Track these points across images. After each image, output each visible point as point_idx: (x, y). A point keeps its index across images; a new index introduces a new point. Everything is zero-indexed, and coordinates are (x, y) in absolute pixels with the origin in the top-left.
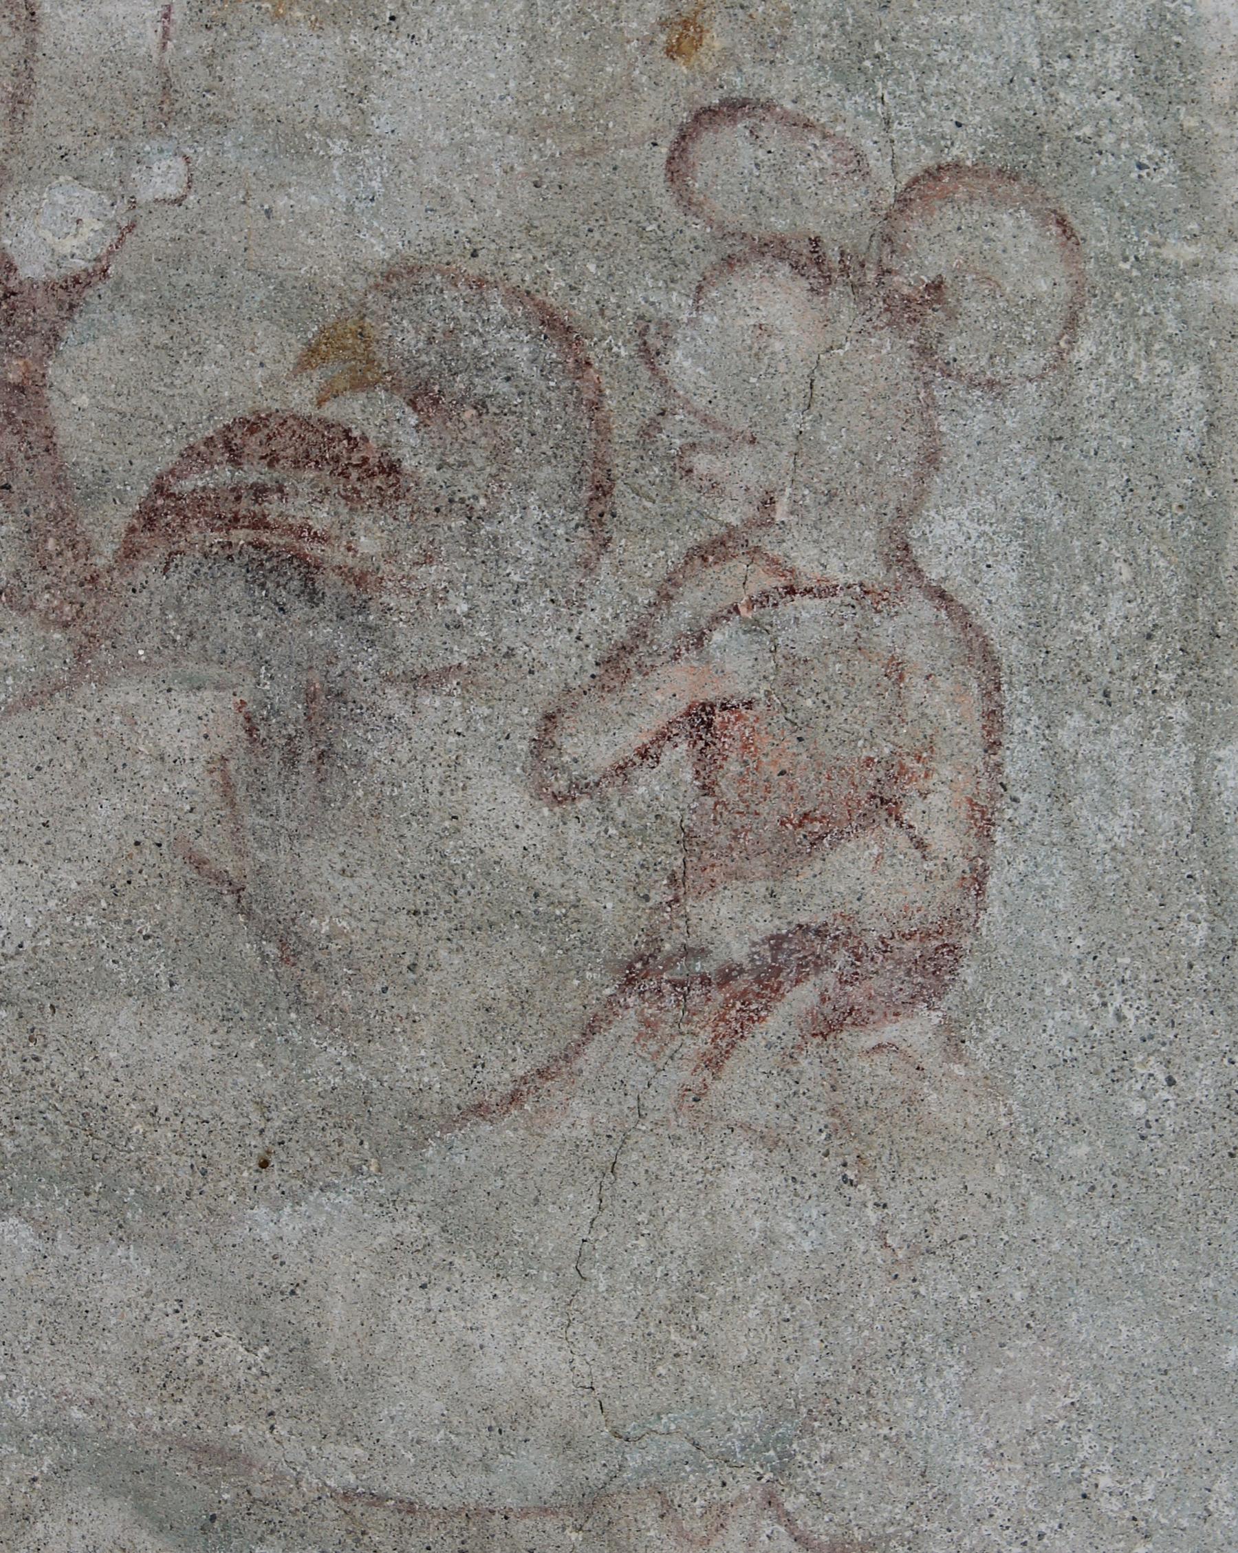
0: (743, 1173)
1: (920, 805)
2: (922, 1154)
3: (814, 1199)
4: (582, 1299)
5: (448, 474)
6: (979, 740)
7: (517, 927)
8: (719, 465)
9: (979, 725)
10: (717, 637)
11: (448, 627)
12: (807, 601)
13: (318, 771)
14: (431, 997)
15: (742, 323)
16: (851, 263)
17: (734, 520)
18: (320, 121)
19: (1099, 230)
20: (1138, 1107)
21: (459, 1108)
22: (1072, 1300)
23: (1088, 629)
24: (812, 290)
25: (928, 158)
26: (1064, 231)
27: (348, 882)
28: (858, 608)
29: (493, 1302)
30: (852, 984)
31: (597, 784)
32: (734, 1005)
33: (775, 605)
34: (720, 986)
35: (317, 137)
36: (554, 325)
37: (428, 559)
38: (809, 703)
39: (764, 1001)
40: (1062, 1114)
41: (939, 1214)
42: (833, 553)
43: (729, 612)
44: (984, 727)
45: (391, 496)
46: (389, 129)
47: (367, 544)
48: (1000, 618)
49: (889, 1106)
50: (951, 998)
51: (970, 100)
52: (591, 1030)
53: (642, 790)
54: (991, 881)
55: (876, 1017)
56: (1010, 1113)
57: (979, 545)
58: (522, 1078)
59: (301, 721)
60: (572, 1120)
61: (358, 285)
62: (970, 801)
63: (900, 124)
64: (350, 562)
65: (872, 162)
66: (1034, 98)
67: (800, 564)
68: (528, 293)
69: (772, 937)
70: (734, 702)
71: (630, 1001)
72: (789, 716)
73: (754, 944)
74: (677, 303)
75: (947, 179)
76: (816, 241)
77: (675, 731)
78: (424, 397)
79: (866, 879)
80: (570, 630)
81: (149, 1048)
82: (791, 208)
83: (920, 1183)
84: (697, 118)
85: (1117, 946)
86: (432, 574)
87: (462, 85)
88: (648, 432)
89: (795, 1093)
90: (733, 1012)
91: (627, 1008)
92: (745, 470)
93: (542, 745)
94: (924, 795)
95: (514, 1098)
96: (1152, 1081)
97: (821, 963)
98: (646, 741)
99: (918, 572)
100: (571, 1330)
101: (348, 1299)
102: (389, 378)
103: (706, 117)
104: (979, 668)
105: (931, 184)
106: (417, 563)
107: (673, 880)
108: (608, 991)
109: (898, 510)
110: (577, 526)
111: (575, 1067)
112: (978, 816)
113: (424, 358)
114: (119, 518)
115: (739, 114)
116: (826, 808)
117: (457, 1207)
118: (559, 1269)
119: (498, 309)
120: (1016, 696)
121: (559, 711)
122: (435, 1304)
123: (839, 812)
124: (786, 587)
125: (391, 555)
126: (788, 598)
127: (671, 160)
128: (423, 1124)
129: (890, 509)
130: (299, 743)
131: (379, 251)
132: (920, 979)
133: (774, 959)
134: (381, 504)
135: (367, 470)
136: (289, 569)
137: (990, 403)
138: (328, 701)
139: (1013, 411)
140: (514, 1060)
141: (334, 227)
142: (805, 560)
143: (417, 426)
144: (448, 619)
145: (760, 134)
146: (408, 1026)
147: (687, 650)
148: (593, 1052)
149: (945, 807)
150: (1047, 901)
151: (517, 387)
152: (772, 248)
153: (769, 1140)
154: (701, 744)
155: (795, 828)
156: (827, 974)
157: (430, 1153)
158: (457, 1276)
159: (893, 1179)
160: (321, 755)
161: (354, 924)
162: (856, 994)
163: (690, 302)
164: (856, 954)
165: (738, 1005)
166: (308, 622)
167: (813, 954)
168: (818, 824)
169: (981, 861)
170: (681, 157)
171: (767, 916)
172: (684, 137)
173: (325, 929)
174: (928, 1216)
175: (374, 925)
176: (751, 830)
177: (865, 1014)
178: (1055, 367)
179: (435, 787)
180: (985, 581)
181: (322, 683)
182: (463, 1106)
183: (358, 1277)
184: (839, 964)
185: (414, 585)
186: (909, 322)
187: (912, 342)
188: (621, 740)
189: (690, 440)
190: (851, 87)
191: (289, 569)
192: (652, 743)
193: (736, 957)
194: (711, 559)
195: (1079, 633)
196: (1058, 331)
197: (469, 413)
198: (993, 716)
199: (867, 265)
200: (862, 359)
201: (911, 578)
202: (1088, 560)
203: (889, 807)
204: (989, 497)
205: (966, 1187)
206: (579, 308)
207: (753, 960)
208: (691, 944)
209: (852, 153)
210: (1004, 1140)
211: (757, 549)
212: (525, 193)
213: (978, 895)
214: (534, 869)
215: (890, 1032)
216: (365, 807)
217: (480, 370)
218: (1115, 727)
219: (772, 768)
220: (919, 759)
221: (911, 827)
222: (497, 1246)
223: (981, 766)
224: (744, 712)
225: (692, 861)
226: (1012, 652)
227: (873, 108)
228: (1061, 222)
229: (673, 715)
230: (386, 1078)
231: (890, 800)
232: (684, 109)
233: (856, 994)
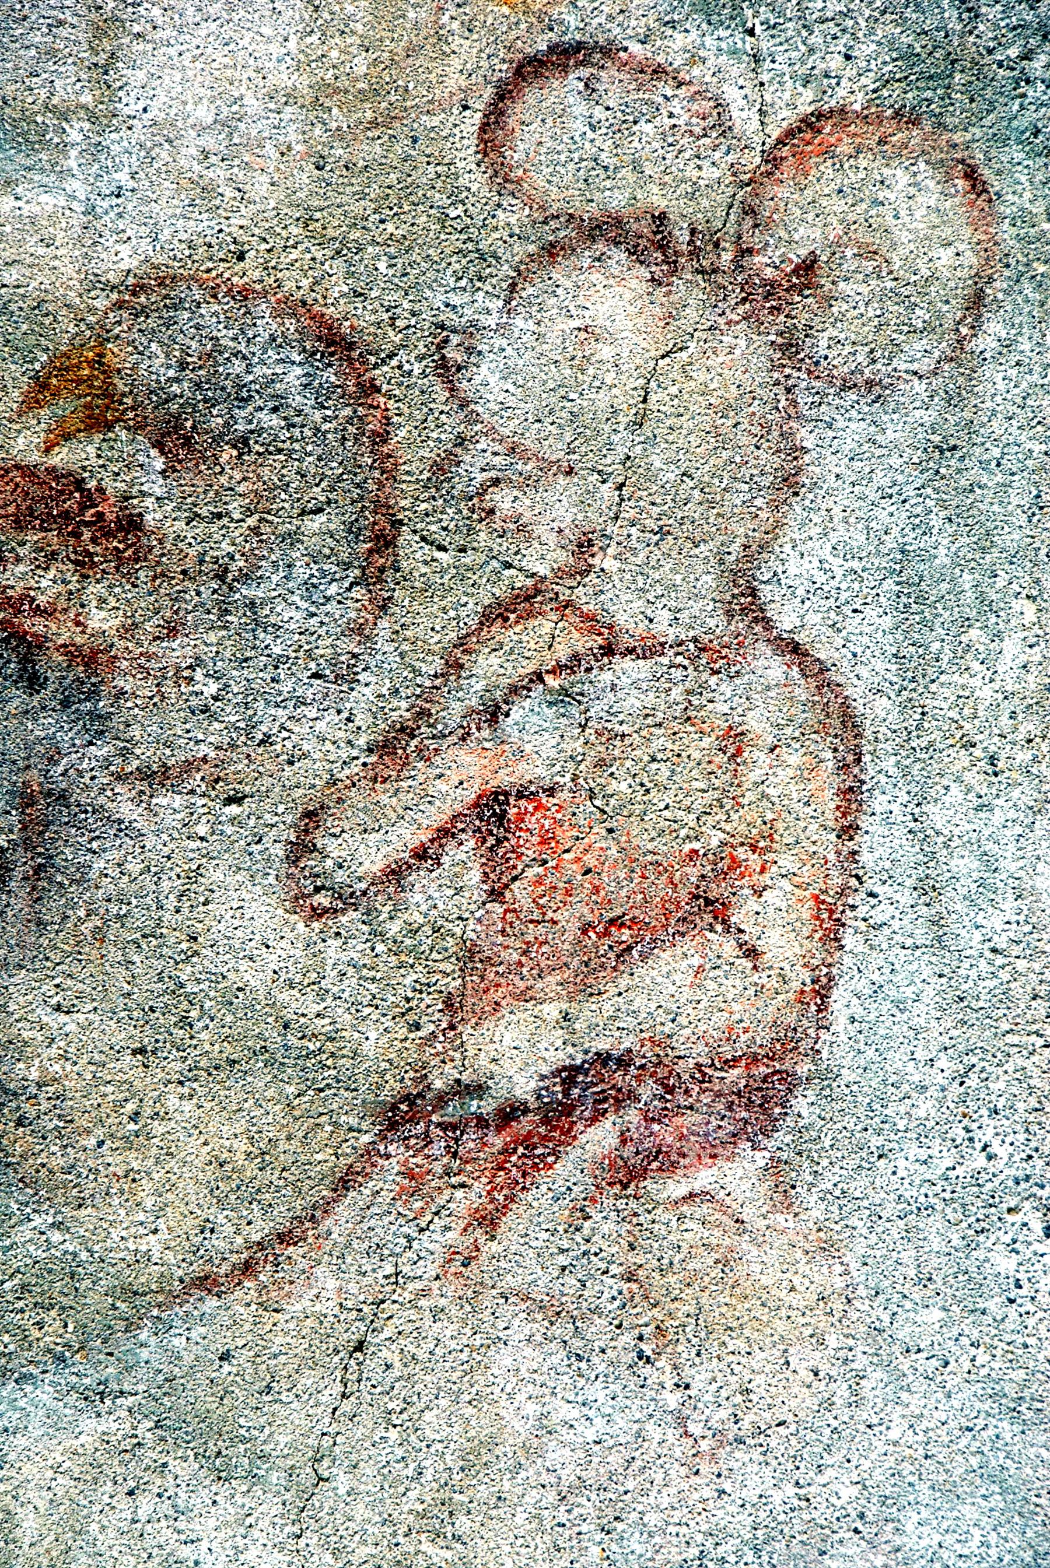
0: (521, 1352)
1: (753, 905)
2: (735, 1324)
3: (601, 1379)
4: (317, 1505)
5: (200, 528)
6: (831, 824)
7: (261, 1064)
8: (528, 502)
9: (832, 805)
10: (516, 714)
11: (193, 713)
12: (628, 663)
13: (34, 888)
14: (154, 1150)
15: (562, 326)
16: (705, 239)
17: (542, 570)
18: (55, 101)
20: (1006, 1264)
21: (181, 1281)
22: (911, 1498)
23: (976, 682)
24: (653, 280)
25: (806, 101)
26: (974, 186)
27: (63, 1018)
28: (691, 668)
29: (213, 1510)
30: (660, 1122)
31: (364, 893)
32: (515, 1150)
33: (589, 670)
34: (499, 1129)
35: (51, 120)
36: (333, 343)
37: (172, 632)
38: (623, 787)
39: (551, 1145)
40: (912, 1273)
41: (752, 1396)
42: (656, 594)
43: (531, 681)
44: (838, 807)
45: (129, 559)
46: (140, 106)
47: (99, 620)
48: (868, 682)
49: (699, 1266)
50: (782, 1137)
51: (863, 24)
52: (344, 1183)
53: (418, 897)
54: (835, 994)
55: (687, 1161)
56: (847, 1272)
57: (844, 586)
58: (259, 1243)
59: (16, 830)
60: (315, 1291)
61: (97, 303)
62: (816, 897)
63: (773, 62)
64: (79, 640)
65: (735, 114)
66: (946, 15)
67: (621, 619)
68: (304, 303)
69: (564, 1068)
70: (533, 789)
71: (391, 1149)
72: (597, 803)
73: (543, 1078)
75: (827, 130)
76: (663, 216)
77: (460, 826)
78: (177, 438)
79: (681, 997)
80: (339, 712)
82: (631, 177)
83: (731, 1358)
84: (519, 72)
85: (989, 1069)
86: (178, 651)
87: (232, 46)
88: (442, 468)
89: (584, 1254)
90: (514, 1159)
91: (388, 1156)
92: (557, 511)
93: (301, 849)
94: (759, 893)
95: (248, 1268)
96: (1025, 1231)
97: (623, 1098)
98: (424, 839)
99: (767, 623)
100: (302, 1542)
101: (42, 1511)
102: (131, 415)
103: (530, 69)
104: (836, 736)
105: (808, 136)
106: (158, 638)
107: (448, 1004)
108: (366, 1139)
109: (746, 547)
110: (352, 585)
111: (322, 1229)
112: (825, 916)
113: (175, 388)
115: (572, 63)
116: (637, 912)
117: (174, 1398)
118: (292, 1467)
119: (266, 325)
120: (881, 766)
121: (322, 808)
122: (142, 1515)
123: (652, 915)
124: (601, 647)
125: (128, 630)
126: (606, 660)
127: (484, 128)
128: (143, 1303)
129: (735, 548)
131: (128, 261)
132: (744, 1114)
133: (566, 1093)
134: (117, 569)
135: (101, 528)
137: (866, 409)
139: (895, 417)
140: (249, 1223)
143: (164, 471)
144: (194, 702)
145: (597, 86)
146: (126, 1187)
147: (479, 729)
148: (343, 1210)
149: (784, 906)
150: (905, 1017)
151: (285, 419)
153: (553, 1311)
154: (491, 841)
155: (599, 937)
156: (633, 1112)
157: (143, 1336)
158: (171, 1480)
159: (698, 1355)
160: (38, 869)
161: (68, 1067)
162: (665, 1134)
163: (500, 303)
164: (665, 1086)
165: (521, 1150)
166: (27, 712)
167: (613, 1087)
168: (627, 931)
169: (825, 970)
170: (497, 122)
171: (559, 1043)
172: (504, 94)
173: (34, 1074)
174: (739, 1399)
175: (93, 1068)
176: (546, 942)
177: (674, 1157)
178: (952, 359)
179: (171, 903)
180: (850, 629)
181: (40, 784)
182: (187, 1279)
183: (54, 1483)
184: (644, 1098)
185: (153, 664)
186: (771, 313)
187: (772, 338)
188: (394, 838)
189: (493, 474)
190: (715, 18)
192: (432, 841)
193: (518, 1092)
194: (512, 617)
195: (964, 687)
196: (959, 314)
197: (227, 454)
198: (851, 795)
199: (723, 244)
200: (709, 362)
201: (758, 629)
202: (982, 598)
203: (718, 911)
204: (860, 526)
205: (788, 1363)
206: (364, 317)
207: (539, 1097)
208: (465, 1078)
209: (712, 104)
210: (838, 1305)
211: (568, 604)
212: (305, 177)
213: (819, 1011)
214: (284, 996)
215: (704, 1178)
216: (86, 928)
217: (243, 399)
218: (1000, 802)
219: (575, 867)
220: (754, 848)
221: (741, 931)
222: (219, 1443)
223: (832, 857)
224: (544, 801)
225: (473, 986)
226: (879, 712)
227: (740, 45)
228: (971, 174)
229: (458, 807)
230: (96, 1248)
231: (717, 900)
232: (504, 61)
233: (665, 1134)
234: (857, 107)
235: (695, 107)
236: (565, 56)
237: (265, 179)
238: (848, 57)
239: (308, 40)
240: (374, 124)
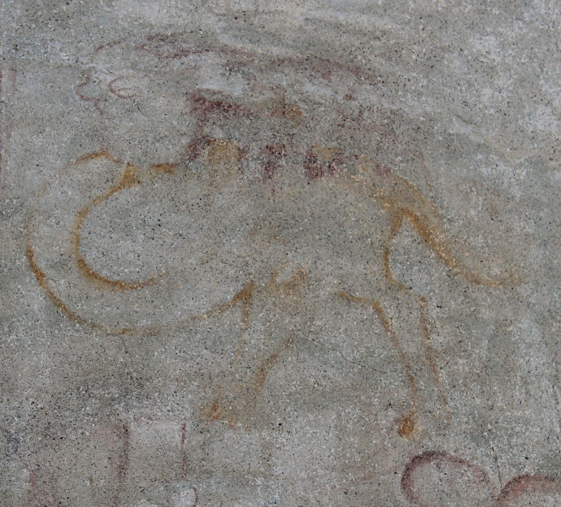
18: (251, 470)
25: (514, 473)
35: (250, 477)
46: (281, 472)
63: (501, 459)
65: (490, 476)
76: (347, 95)
82: (457, 498)
84: (413, 461)
103: (417, 460)
115: (431, 458)
127: (403, 479)
170: (407, 478)
209: (481, 473)
227: (489, 453)
234: (532, 475)
235: (476, 474)
236: (429, 455)
237: (327, 498)
238: (527, 458)
239: (338, 450)
240: (365, 479)
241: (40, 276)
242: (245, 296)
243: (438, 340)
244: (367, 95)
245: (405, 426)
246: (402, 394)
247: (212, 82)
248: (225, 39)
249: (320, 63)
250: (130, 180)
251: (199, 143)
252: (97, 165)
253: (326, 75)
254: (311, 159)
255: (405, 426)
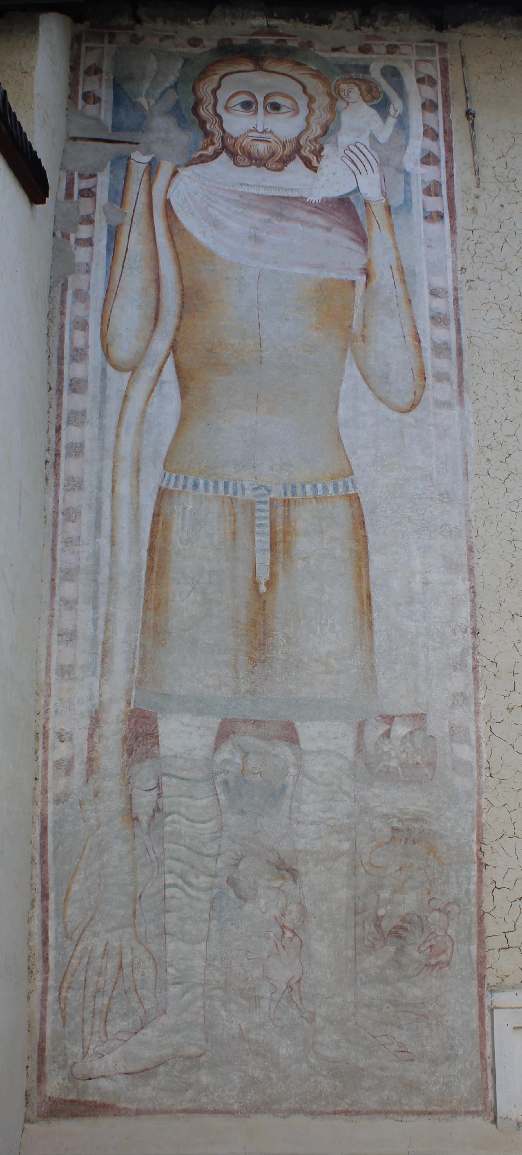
19: (462, 906)
36: (419, 917)
42: (441, 933)
48: (454, 937)
74: (429, 914)
78: (409, 923)
79: (443, 958)
81: (390, 972)
93: (419, 949)
103: (431, 899)
114: (387, 934)
120: (455, 943)
130: (401, 950)
136: (399, 937)
138: (403, 947)
141: (402, 910)
142: (438, 933)
152: (436, 910)
172: (429, 901)
191: (399, 937)
198: (453, 945)
225: (430, 957)
226: (454, 940)
236: (433, 898)
241: (363, 866)
242: (401, 869)
243: (436, 876)
244: (425, 826)
245: (429, 893)
246: (428, 887)
247: (395, 824)
248: (398, 815)
249: (416, 820)
250: (380, 846)
251: (393, 837)
252: (374, 843)
253: (417, 822)
254: (414, 840)
255: (429, 893)
